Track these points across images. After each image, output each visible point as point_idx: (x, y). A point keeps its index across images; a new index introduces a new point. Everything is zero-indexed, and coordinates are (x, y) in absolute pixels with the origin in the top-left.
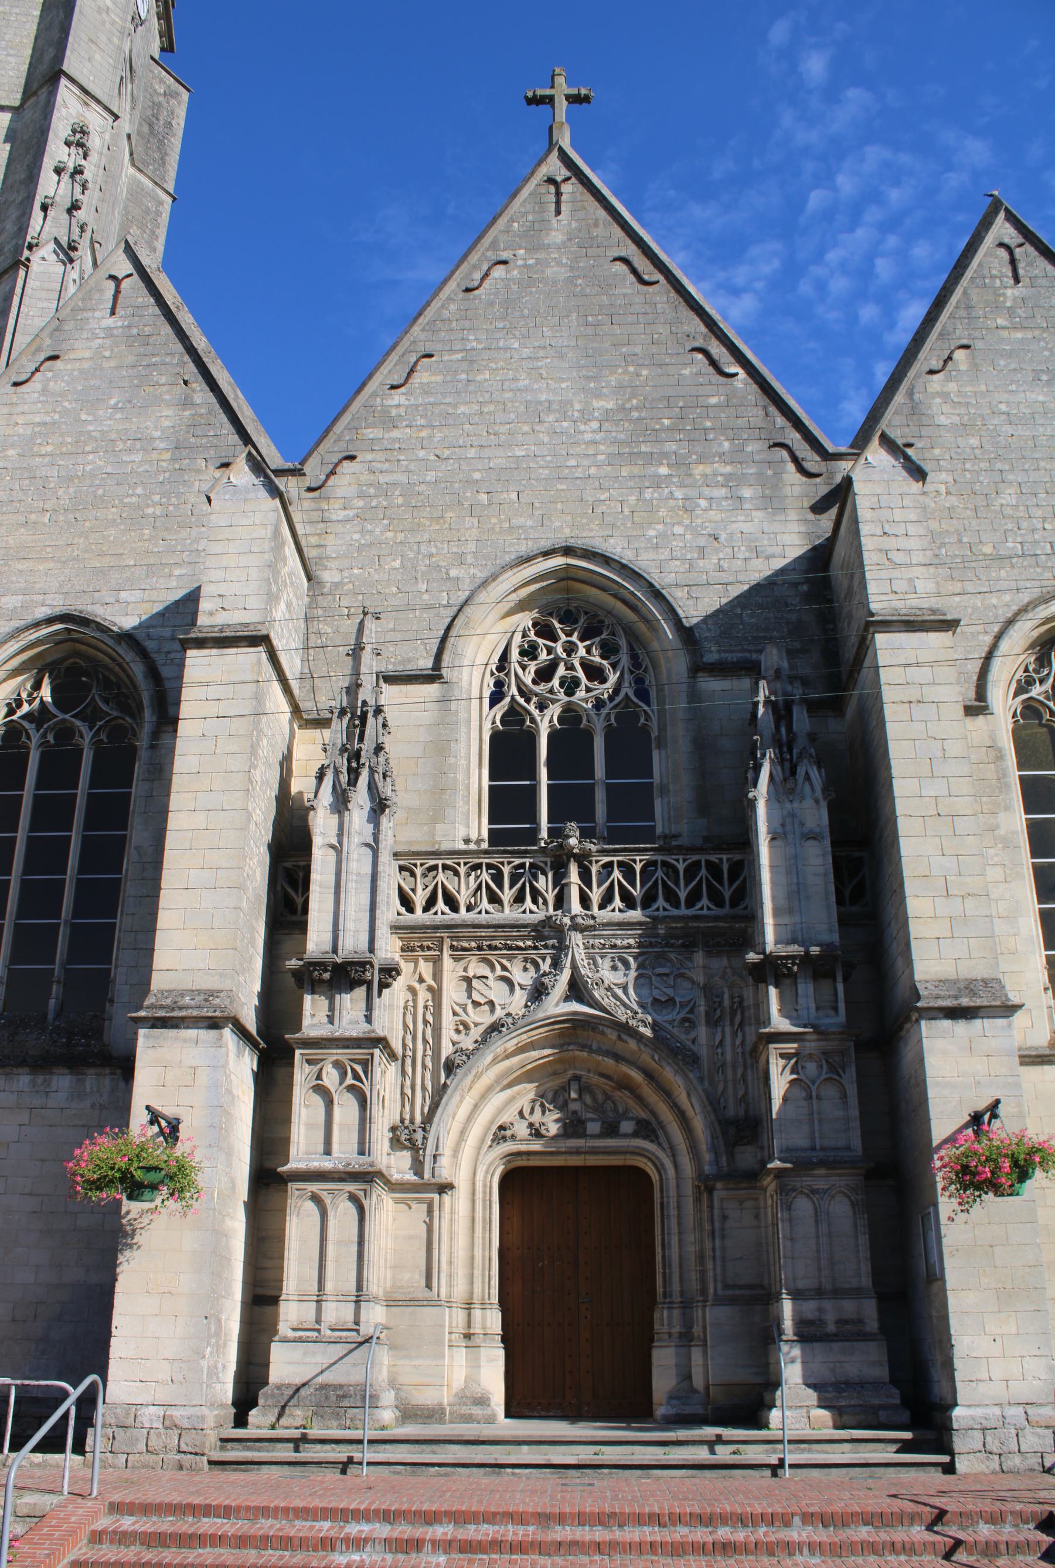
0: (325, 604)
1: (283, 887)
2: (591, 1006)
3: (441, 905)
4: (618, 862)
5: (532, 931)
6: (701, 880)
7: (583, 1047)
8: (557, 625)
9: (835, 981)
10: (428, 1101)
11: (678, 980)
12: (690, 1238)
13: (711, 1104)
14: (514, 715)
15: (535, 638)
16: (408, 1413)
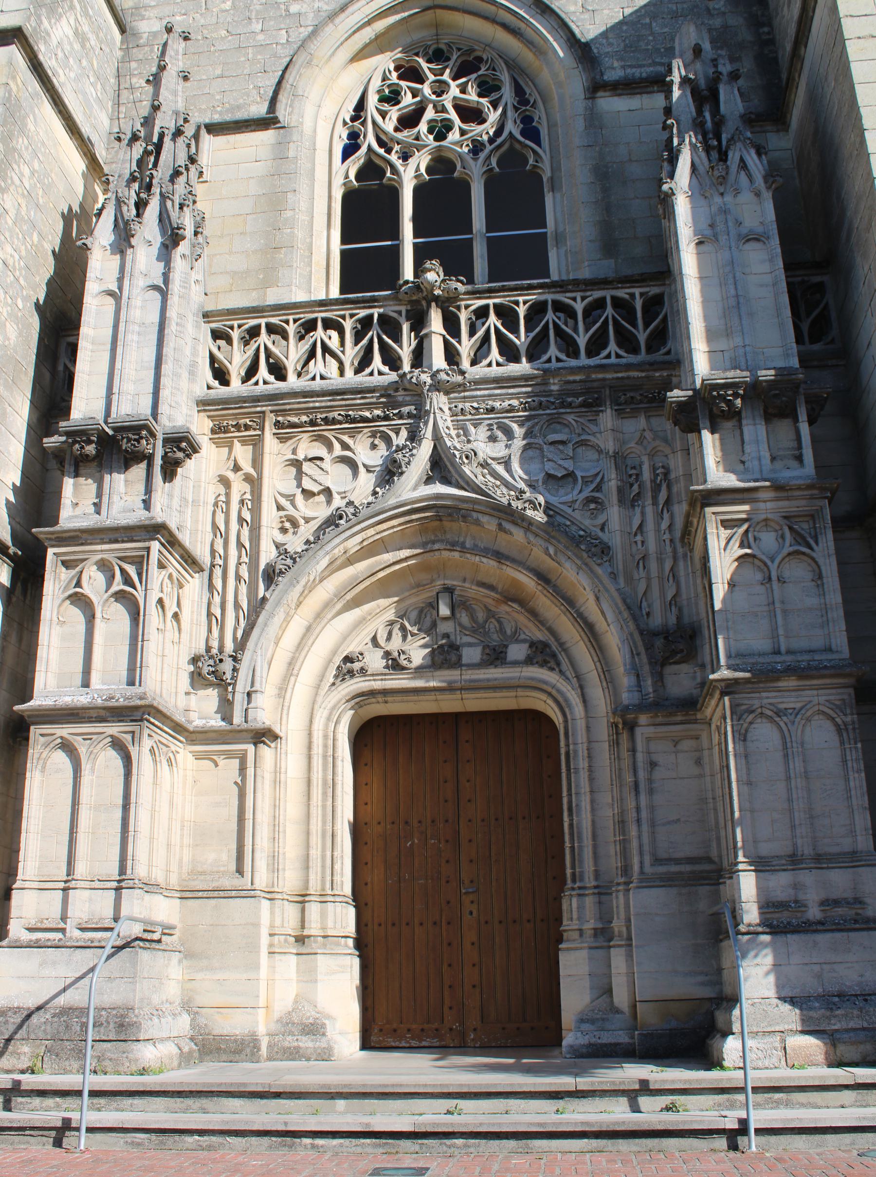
0: (141, 57)
1: (65, 365)
2: (466, 490)
3: (263, 372)
4: (495, 305)
5: (382, 396)
6: (606, 321)
7: (453, 545)
8: (425, 65)
9: (796, 420)
10: (243, 623)
11: (580, 450)
12: (605, 798)
13: (629, 608)
14: (371, 170)
15: (397, 81)
16: (208, 1046)
